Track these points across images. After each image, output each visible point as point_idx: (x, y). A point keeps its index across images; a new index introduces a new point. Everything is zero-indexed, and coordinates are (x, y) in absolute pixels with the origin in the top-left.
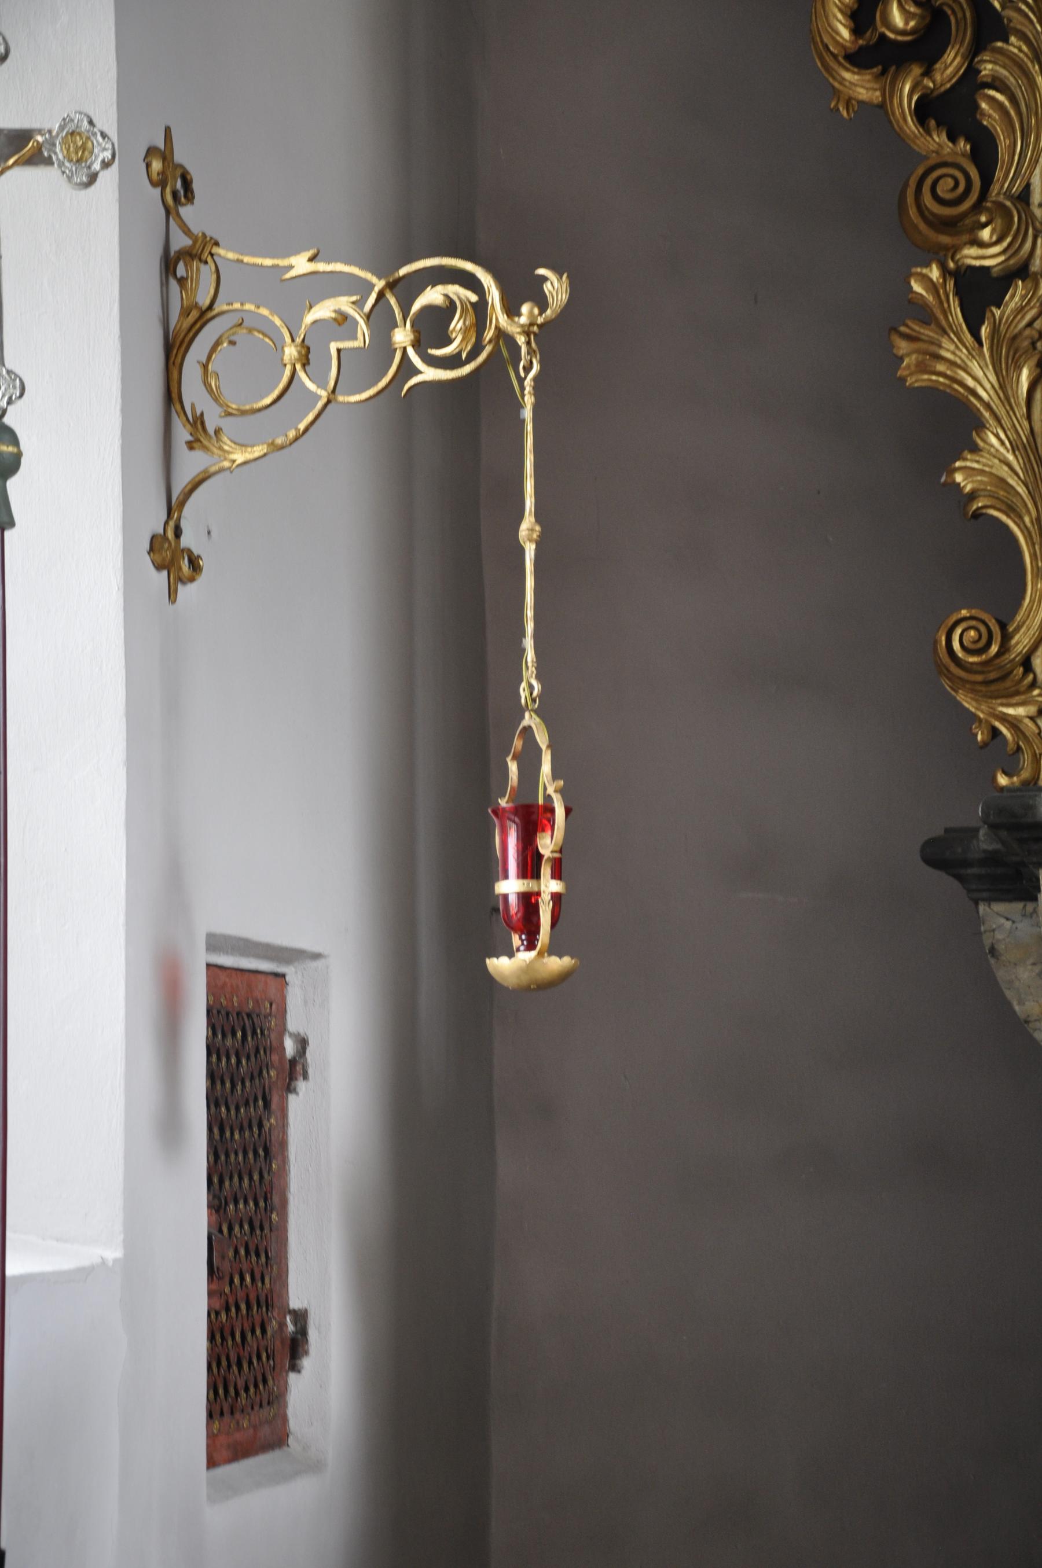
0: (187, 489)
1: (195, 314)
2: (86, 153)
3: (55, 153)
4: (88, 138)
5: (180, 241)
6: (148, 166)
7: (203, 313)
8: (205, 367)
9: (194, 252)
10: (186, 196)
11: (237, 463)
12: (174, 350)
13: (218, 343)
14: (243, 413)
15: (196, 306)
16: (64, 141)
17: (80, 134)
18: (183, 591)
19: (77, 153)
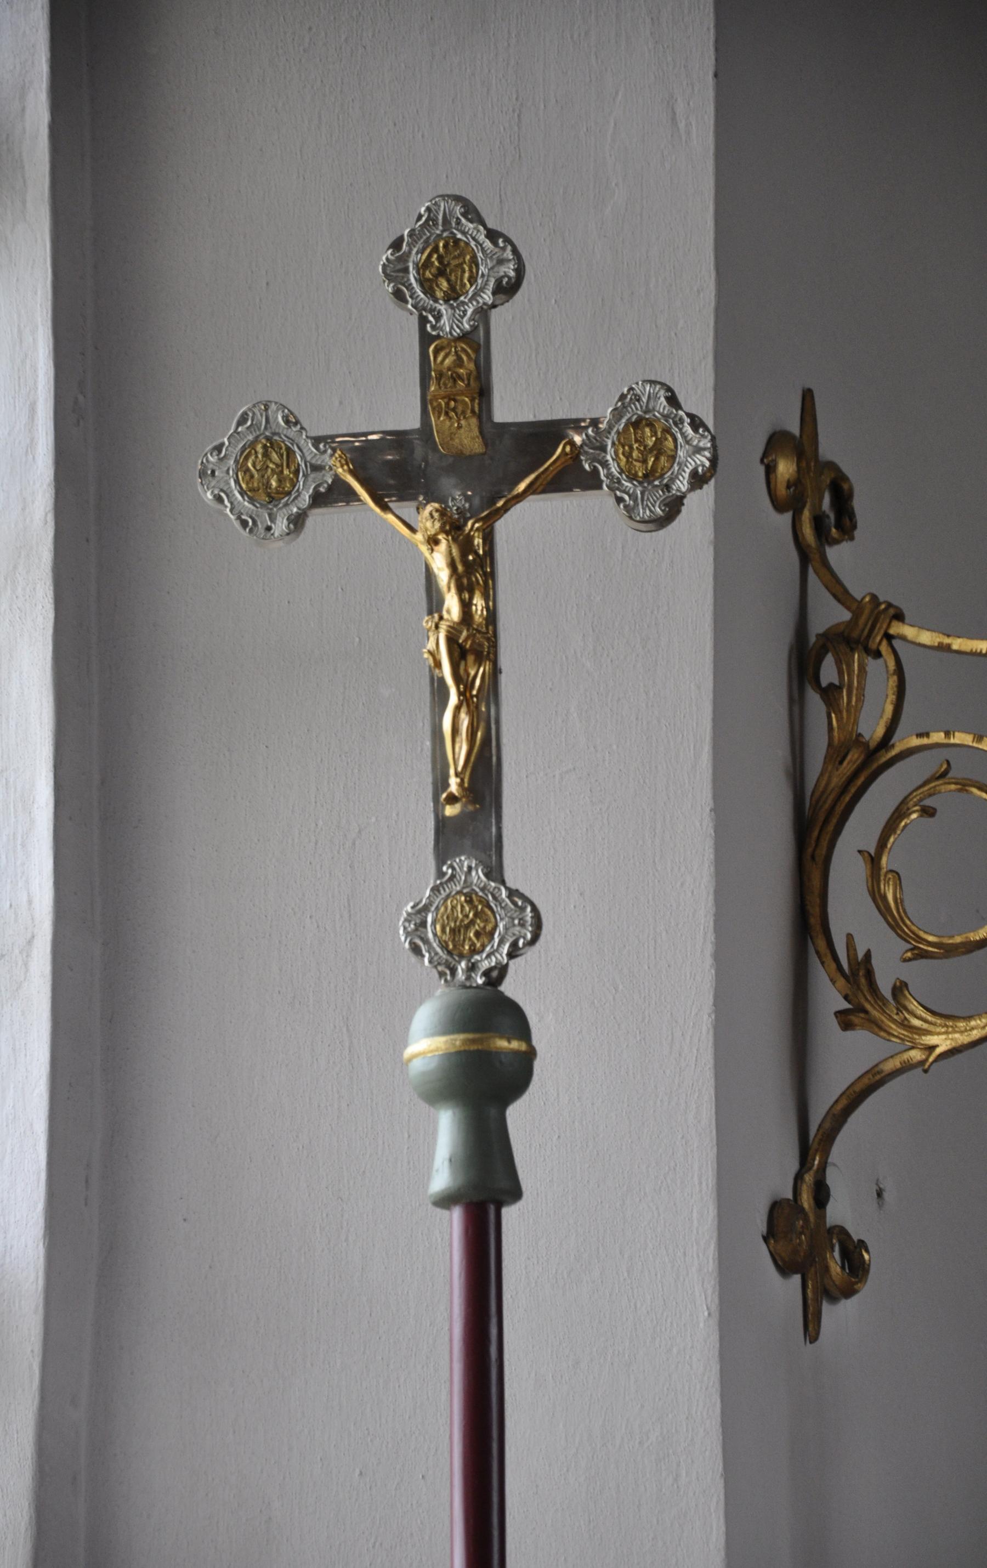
0: (839, 1107)
1: (855, 757)
2: (663, 459)
3: (605, 464)
4: (667, 431)
5: (828, 614)
6: (770, 470)
7: (872, 753)
8: (874, 861)
9: (855, 634)
10: (839, 526)
11: (938, 1051)
12: (813, 829)
13: (899, 813)
14: (949, 951)
15: (858, 741)
16: (623, 439)
17: (650, 424)
18: (836, 1316)
19: (645, 461)
